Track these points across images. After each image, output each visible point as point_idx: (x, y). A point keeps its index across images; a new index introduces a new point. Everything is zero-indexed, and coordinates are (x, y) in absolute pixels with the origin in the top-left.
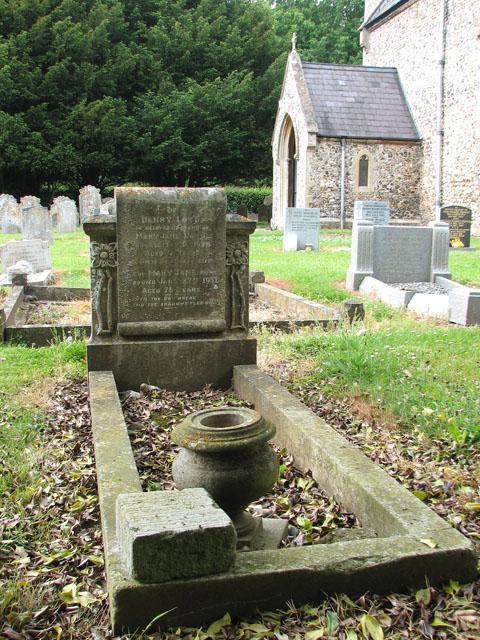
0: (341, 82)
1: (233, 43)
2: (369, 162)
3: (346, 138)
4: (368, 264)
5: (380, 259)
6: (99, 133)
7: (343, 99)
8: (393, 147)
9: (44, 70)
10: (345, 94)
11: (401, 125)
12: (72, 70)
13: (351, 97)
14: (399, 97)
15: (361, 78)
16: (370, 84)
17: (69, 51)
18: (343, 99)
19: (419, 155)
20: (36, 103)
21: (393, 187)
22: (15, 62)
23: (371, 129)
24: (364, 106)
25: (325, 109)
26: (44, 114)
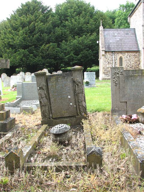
0: (116, 34)
1: (91, 24)
2: (123, 59)
3: (114, 51)
4: (20, 94)
5: (25, 93)
6: (48, 53)
7: (116, 39)
8: (130, 53)
9: (33, 37)
10: (117, 38)
11: (134, 46)
12: (40, 36)
13: (118, 39)
14: (135, 37)
15: (123, 32)
16: (125, 34)
17: (39, 31)
18: (116, 39)
19: (139, 56)
20: (31, 46)
21: (131, 66)
22: (25, 35)
23: (123, 48)
24: (123, 41)
25: (109, 43)
26: (34, 49)
